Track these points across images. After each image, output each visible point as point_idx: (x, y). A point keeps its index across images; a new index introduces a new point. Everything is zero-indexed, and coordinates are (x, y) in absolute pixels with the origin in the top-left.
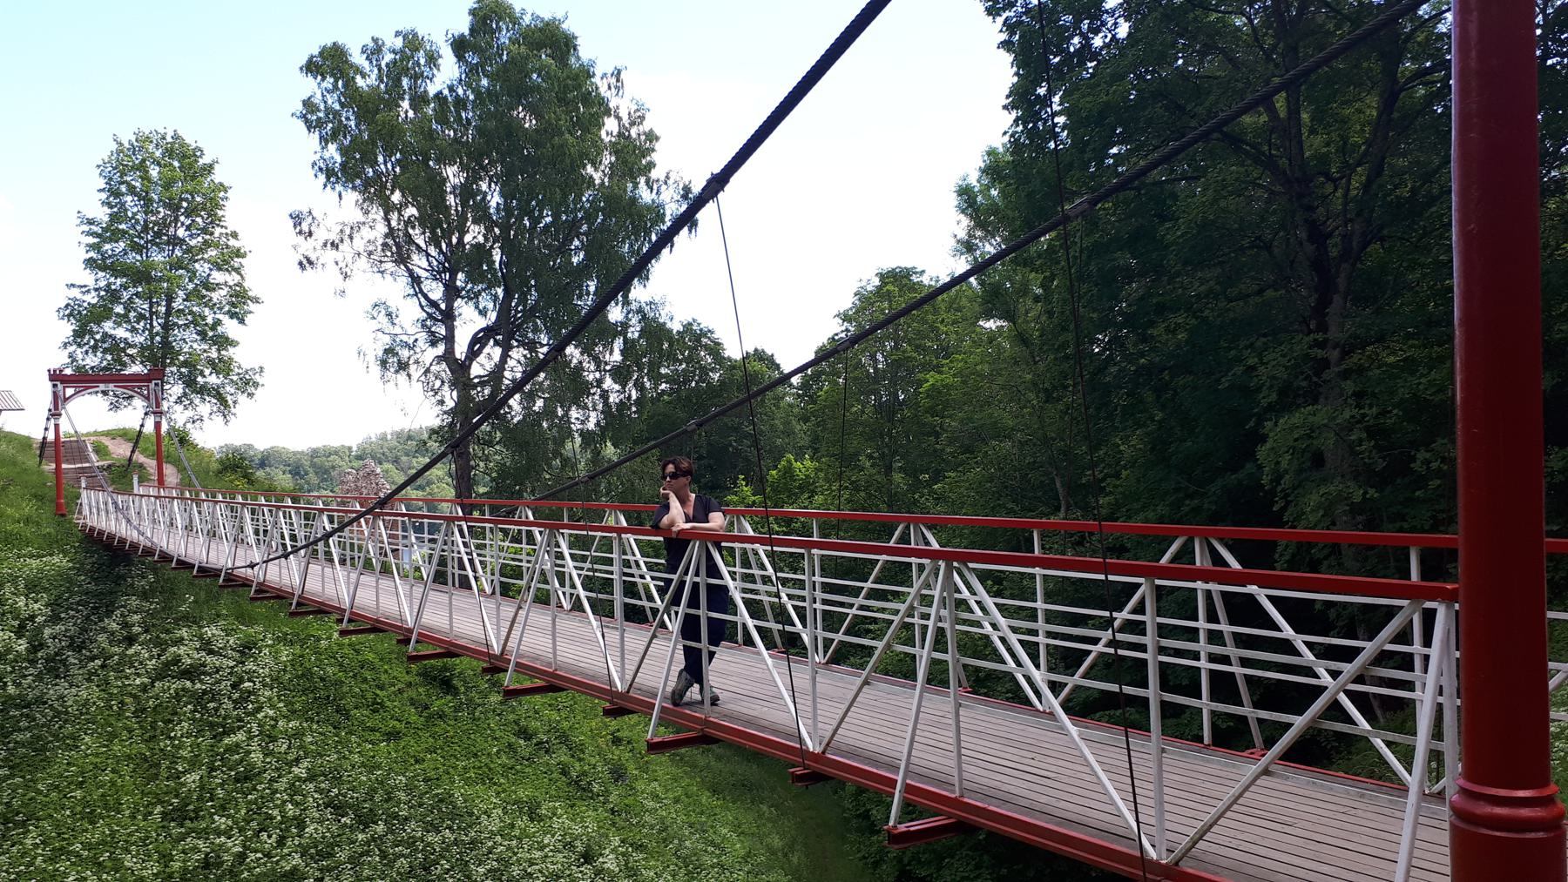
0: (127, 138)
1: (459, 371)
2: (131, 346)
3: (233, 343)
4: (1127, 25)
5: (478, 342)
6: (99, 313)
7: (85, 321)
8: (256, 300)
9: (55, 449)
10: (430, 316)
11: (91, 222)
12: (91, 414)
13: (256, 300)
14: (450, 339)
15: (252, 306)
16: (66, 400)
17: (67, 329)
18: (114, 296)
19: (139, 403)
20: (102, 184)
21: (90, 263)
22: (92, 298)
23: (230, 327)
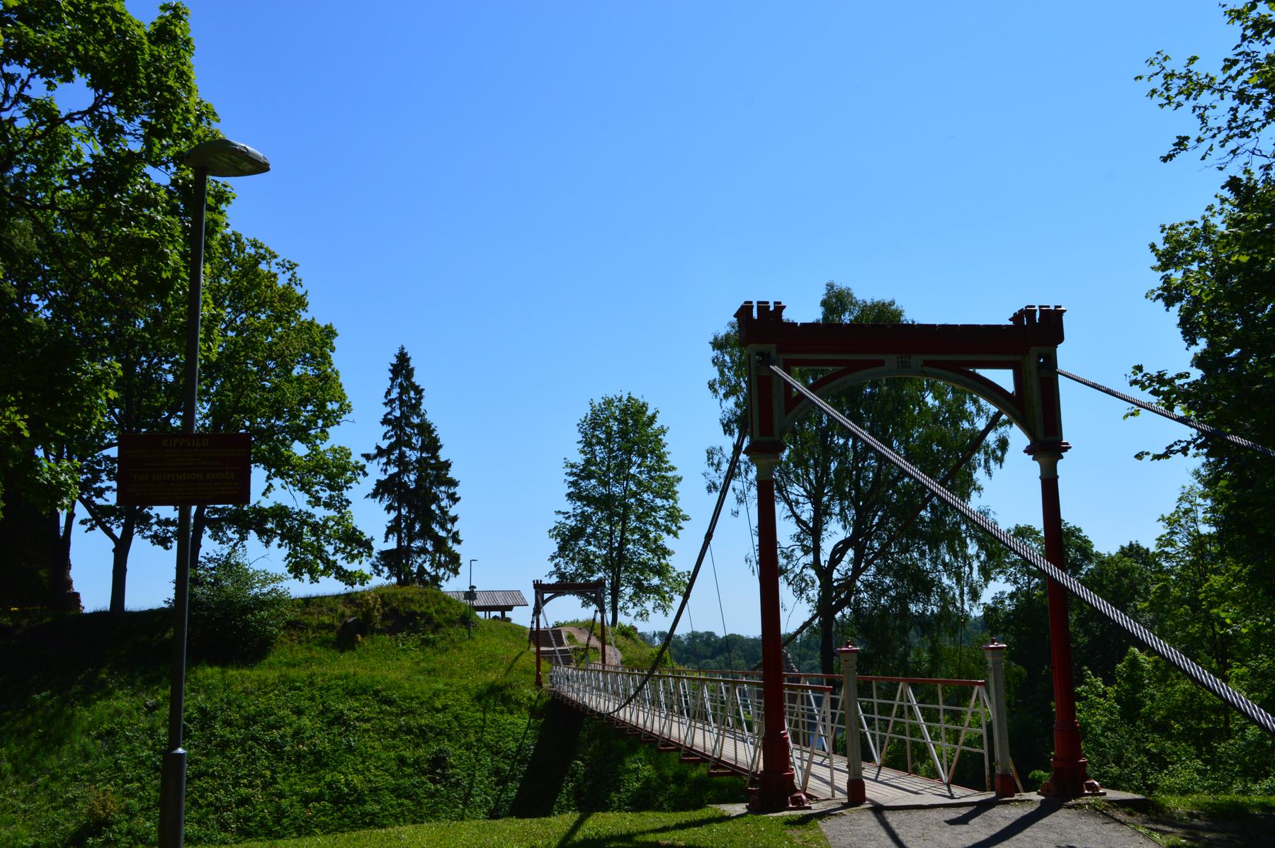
0: (598, 401)
1: (824, 573)
2: (597, 557)
3: (668, 553)
4: (930, 405)
5: (838, 552)
6: (576, 533)
7: (568, 539)
8: (685, 518)
9: (538, 636)
10: (803, 531)
11: (572, 466)
12: (567, 610)
13: (685, 518)
14: (816, 550)
15: (682, 524)
16: (544, 602)
17: (553, 546)
18: (586, 518)
19: (594, 607)
20: (580, 437)
21: (570, 496)
22: (571, 522)
23: (668, 541)
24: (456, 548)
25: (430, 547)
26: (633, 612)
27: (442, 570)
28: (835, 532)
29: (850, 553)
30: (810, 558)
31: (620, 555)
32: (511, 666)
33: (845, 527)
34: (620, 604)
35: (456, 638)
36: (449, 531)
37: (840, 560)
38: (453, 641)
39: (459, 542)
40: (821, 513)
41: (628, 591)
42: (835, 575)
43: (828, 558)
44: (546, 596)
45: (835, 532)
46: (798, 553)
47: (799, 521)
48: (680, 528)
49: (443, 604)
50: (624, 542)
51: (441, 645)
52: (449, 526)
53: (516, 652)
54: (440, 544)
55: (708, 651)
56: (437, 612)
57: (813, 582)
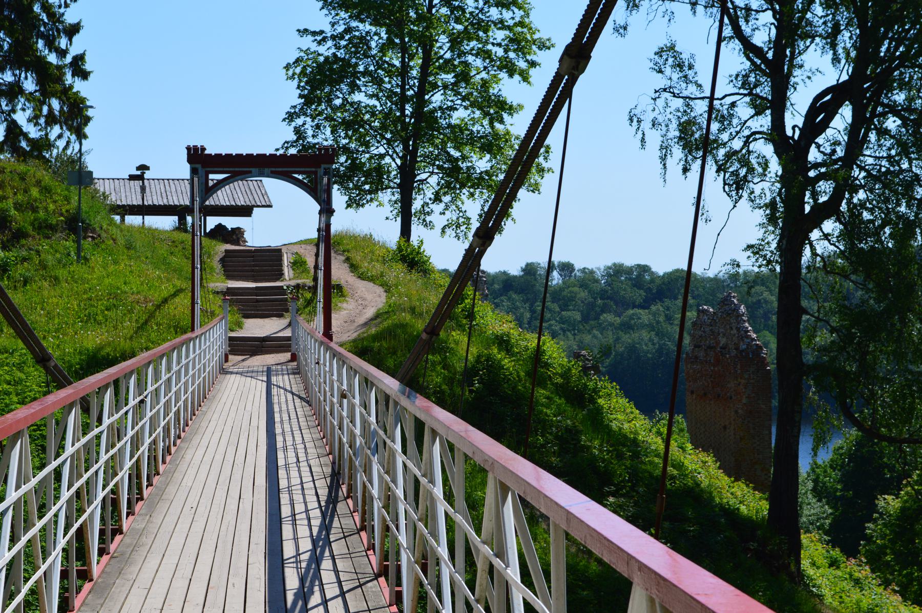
1: (792, 151)
7: (320, 79)
10: (755, 68)
14: (777, 105)
17: (290, 95)
22: (326, 50)
24: (79, 86)
25: (30, 85)
26: (439, 220)
27: (56, 130)
28: (818, 70)
29: (846, 113)
30: (764, 122)
31: (418, 113)
32: (152, 315)
33: (836, 60)
34: (417, 205)
35: (50, 259)
36: (62, 53)
37: (825, 125)
38: (43, 266)
39: (85, 75)
40: (791, 31)
41: (433, 181)
42: (814, 155)
43: (800, 122)
44: (215, 177)
45: (818, 70)
46: (744, 111)
47: (749, 48)
48: (533, 64)
49: (35, 192)
50: (426, 86)
51: (19, 271)
52: (63, 42)
53: (166, 289)
54: (49, 80)
55: (639, 295)
56: (18, 206)
57: (765, 165)
